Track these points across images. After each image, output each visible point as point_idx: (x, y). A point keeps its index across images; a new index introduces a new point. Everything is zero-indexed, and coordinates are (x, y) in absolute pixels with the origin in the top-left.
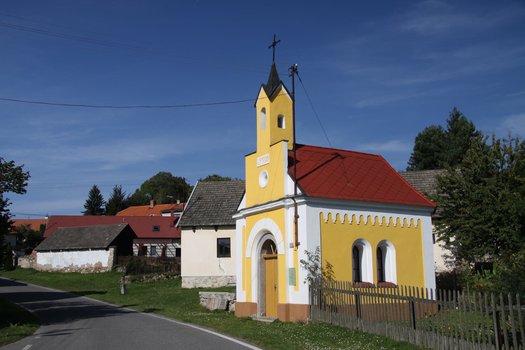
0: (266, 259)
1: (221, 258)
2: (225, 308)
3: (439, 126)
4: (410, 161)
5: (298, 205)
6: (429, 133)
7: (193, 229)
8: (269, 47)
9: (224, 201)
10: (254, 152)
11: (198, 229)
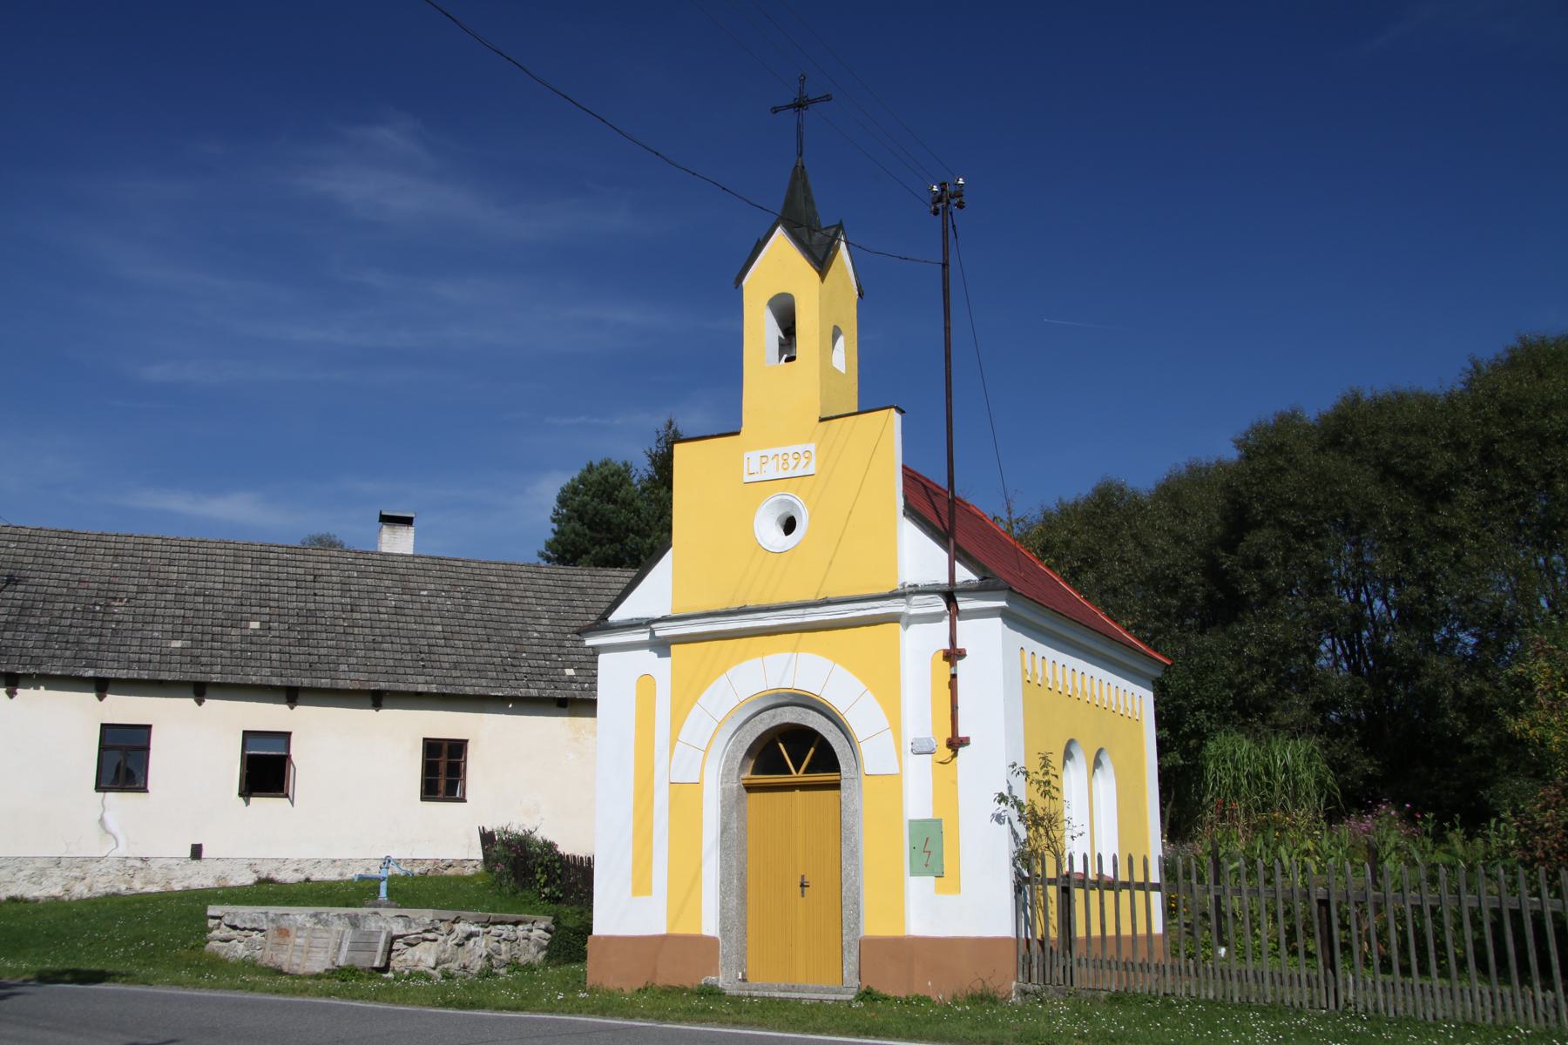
0: (750, 788)
1: (111, 796)
2: (381, 960)
3: (625, 464)
4: (547, 550)
5: (960, 620)
6: (610, 479)
7: (6, 685)
8: (775, 108)
9: (115, 599)
10: (731, 430)
11: (27, 687)
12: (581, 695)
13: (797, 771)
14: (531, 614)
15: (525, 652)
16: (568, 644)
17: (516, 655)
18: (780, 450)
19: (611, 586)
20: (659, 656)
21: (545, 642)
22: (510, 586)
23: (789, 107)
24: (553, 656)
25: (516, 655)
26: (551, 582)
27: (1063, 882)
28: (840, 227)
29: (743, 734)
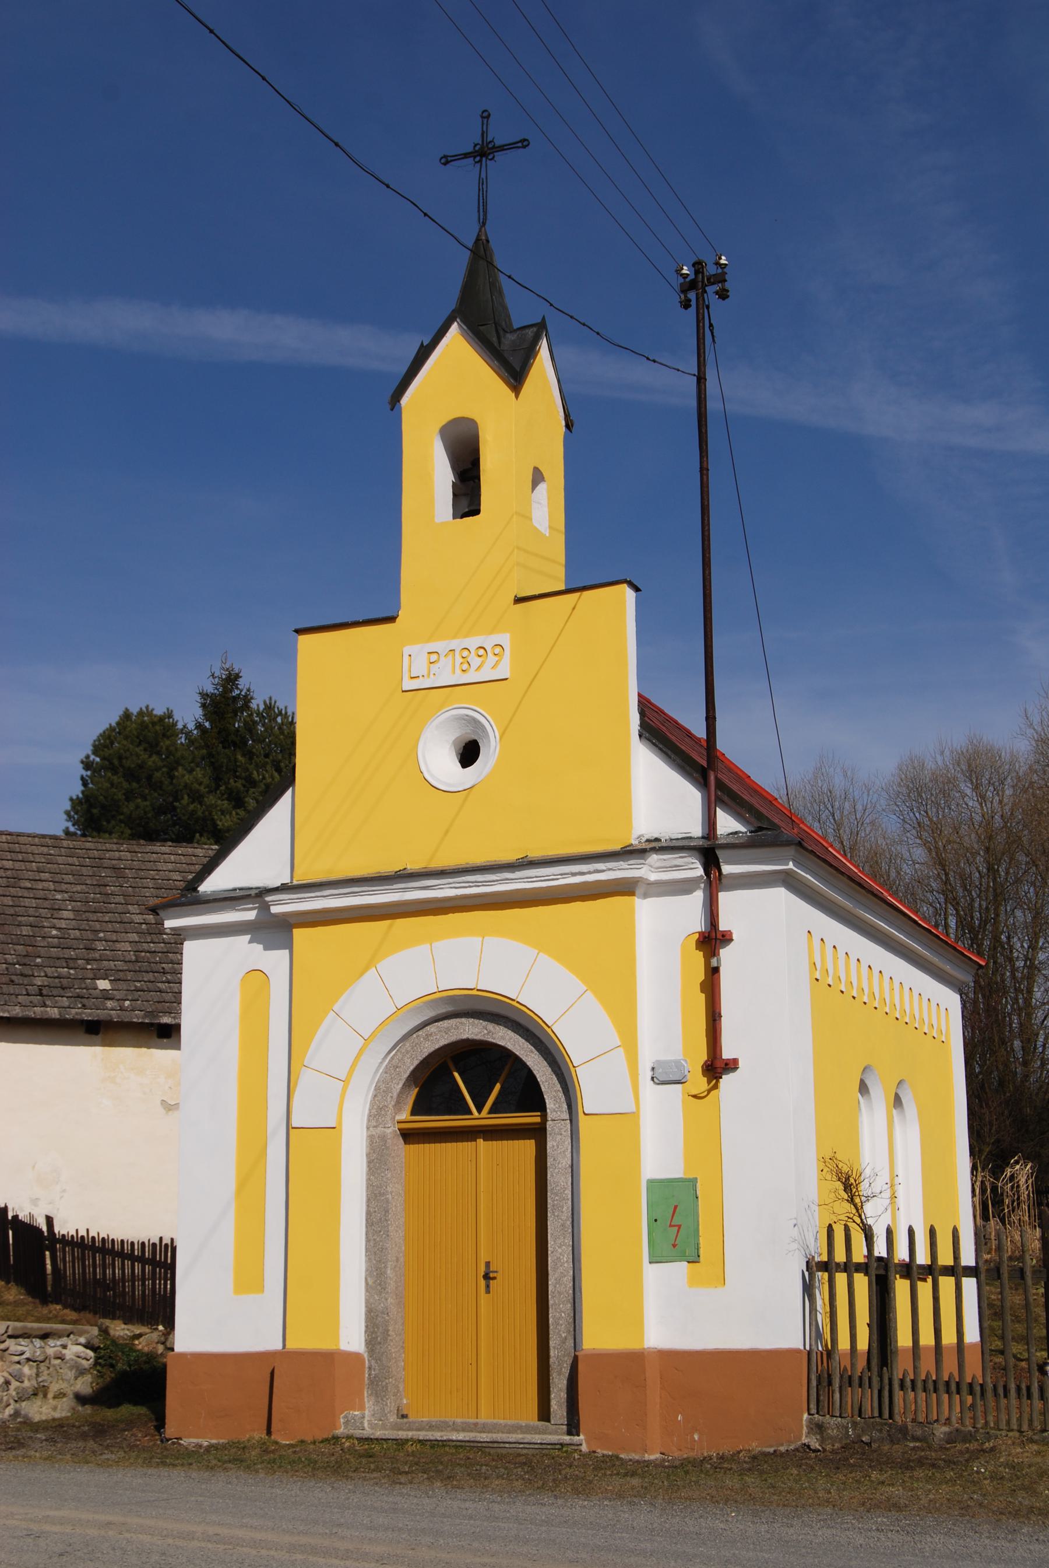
8: (445, 157)
12: (119, 1016)
13: (479, 1111)
14: (47, 904)
15: (39, 957)
16: (100, 946)
17: (26, 960)
18: (456, 644)
19: (160, 866)
20: (266, 949)
21: (70, 943)
22: (18, 865)
23: (466, 156)
24: (80, 962)
25: (26, 960)
26: (75, 861)
27: (877, 1268)
28: (541, 327)
29: (400, 1056)
